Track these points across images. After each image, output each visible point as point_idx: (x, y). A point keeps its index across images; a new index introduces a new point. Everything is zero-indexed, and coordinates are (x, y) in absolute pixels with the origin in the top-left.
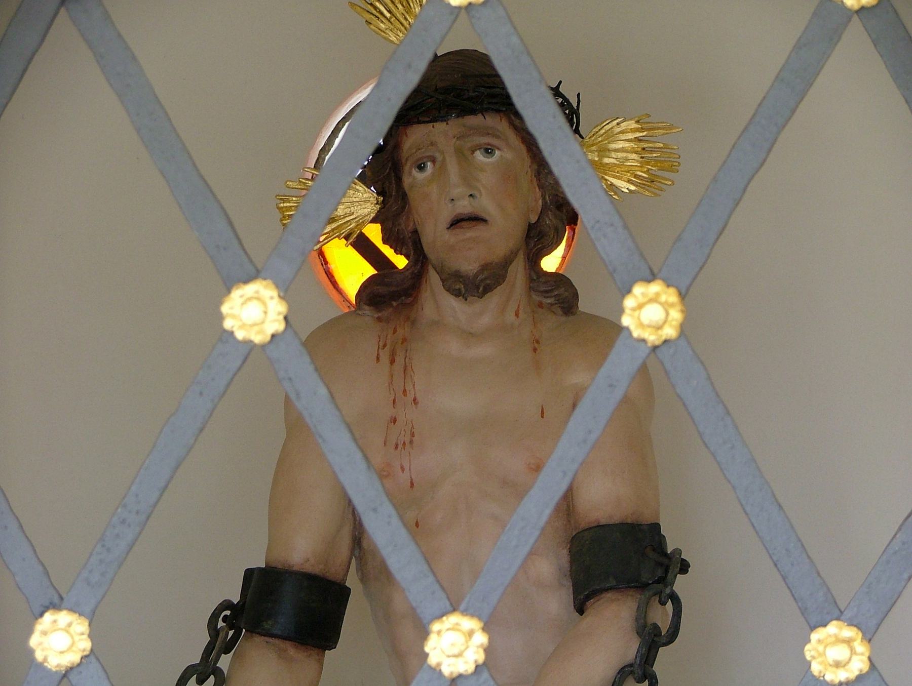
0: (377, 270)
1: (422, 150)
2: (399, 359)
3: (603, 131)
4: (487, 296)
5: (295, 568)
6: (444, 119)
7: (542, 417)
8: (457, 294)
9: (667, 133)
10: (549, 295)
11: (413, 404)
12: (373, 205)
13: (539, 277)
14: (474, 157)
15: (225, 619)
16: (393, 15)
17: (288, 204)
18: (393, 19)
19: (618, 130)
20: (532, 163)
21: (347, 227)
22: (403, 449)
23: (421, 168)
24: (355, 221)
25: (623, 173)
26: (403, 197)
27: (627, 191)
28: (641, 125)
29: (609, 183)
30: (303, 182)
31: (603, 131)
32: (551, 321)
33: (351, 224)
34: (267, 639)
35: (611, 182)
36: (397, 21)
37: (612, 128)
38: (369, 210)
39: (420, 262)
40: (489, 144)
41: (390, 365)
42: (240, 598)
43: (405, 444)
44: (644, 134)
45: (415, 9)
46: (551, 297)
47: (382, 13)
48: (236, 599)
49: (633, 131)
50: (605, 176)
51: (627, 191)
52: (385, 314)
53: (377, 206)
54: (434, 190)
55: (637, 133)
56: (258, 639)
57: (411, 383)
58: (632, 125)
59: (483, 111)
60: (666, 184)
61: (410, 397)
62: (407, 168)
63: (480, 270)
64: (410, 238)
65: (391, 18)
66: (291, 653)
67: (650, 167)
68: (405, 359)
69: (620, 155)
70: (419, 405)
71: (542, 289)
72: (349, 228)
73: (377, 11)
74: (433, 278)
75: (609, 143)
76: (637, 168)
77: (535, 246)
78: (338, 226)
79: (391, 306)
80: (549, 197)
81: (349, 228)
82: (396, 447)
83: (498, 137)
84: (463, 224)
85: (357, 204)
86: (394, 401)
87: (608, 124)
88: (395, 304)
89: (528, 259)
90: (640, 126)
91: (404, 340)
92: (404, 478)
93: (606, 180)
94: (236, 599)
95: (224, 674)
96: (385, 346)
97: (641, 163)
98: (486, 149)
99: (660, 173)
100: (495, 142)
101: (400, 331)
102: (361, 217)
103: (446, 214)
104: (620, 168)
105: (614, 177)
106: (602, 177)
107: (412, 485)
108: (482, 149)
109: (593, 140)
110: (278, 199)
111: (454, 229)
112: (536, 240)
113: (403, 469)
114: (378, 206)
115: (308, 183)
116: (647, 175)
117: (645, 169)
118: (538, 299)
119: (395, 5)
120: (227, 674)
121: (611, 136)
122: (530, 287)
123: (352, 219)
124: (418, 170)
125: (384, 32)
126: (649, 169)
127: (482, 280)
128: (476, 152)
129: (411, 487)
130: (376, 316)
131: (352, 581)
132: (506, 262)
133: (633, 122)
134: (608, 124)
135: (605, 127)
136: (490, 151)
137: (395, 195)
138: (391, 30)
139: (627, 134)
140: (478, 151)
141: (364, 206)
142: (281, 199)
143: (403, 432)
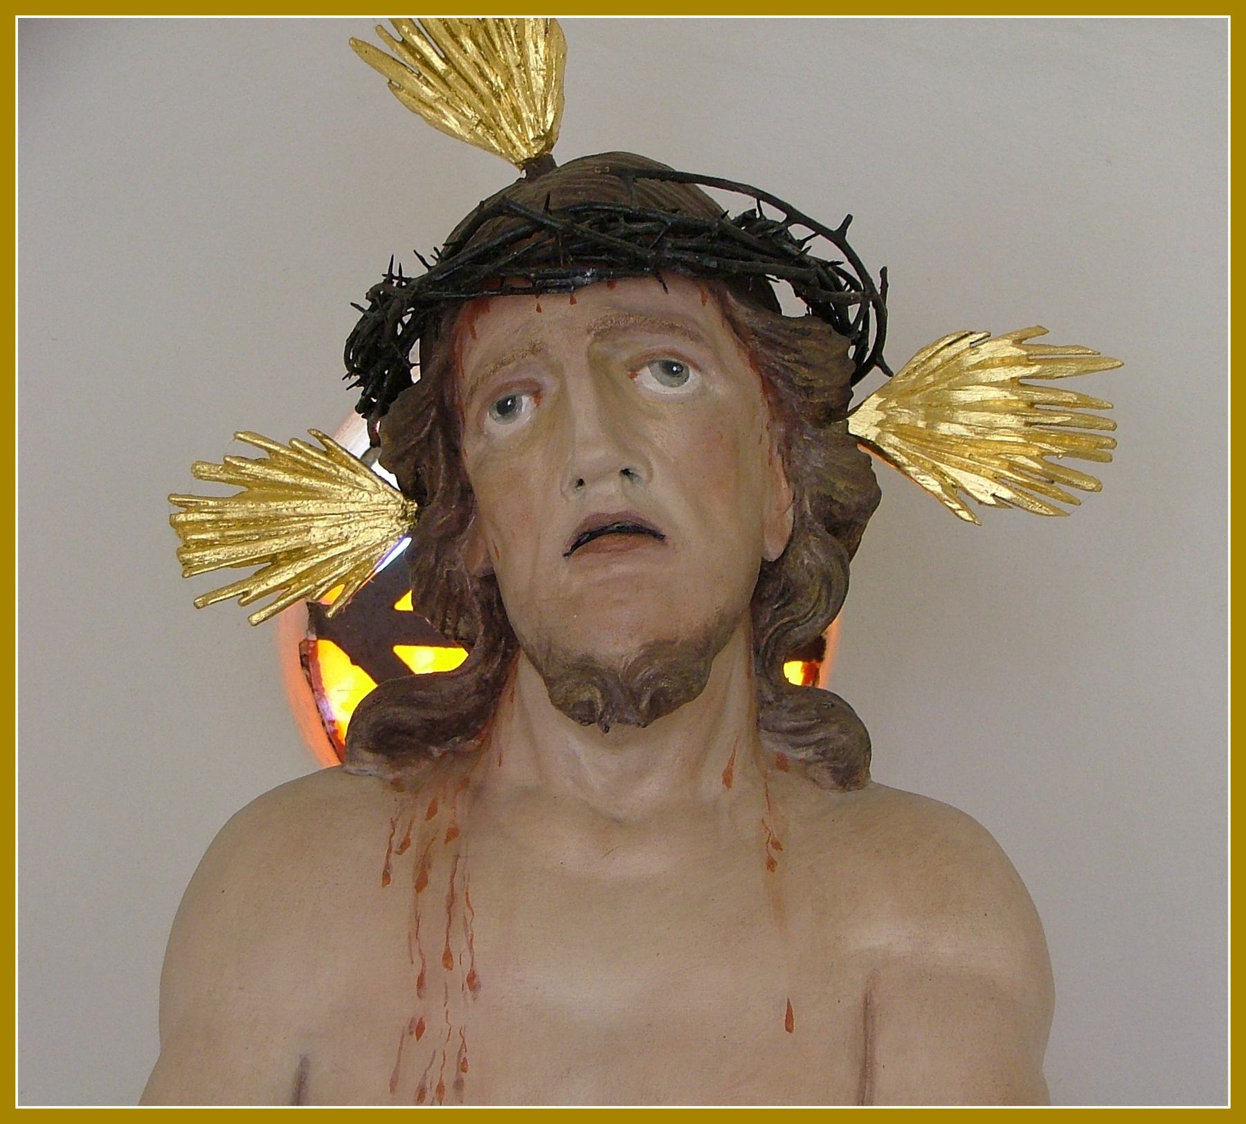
0: (397, 660)
1: (510, 366)
2: (438, 878)
3: (937, 361)
6: (567, 288)
7: (789, 1029)
8: (585, 715)
9: (1087, 372)
10: (802, 739)
11: (466, 986)
12: (393, 521)
13: (779, 697)
16: (455, 68)
17: (197, 517)
18: (452, 77)
19: (974, 359)
20: (773, 419)
23: (506, 409)
25: (982, 459)
27: (992, 501)
28: (1027, 351)
29: (949, 481)
31: (937, 361)
33: (341, 565)
35: (954, 480)
37: (958, 355)
38: (385, 532)
39: (501, 654)
40: (672, 353)
44: (1034, 369)
45: (504, 51)
46: (808, 745)
47: (427, 64)
49: (1005, 362)
50: (942, 466)
51: (992, 501)
52: (411, 773)
54: (536, 463)
55: (1018, 368)
58: (1008, 349)
59: (659, 271)
60: (1084, 489)
61: (461, 970)
62: (471, 414)
63: (643, 656)
64: (476, 593)
67: (1046, 446)
68: (452, 877)
69: (976, 417)
70: (481, 993)
71: (787, 725)
72: (337, 572)
73: (415, 58)
75: (951, 388)
76: (1016, 449)
78: (312, 568)
81: (337, 572)
83: (696, 338)
84: (604, 540)
85: (358, 518)
87: (950, 344)
88: (436, 751)
89: (757, 652)
91: (453, 833)
93: (943, 474)
96: (405, 845)
97: (1025, 436)
99: (1068, 462)
100: (686, 348)
101: (444, 812)
102: (365, 549)
104: (976, 447)
105: (962, 467)
106: (934, 467)
108: (656, 365)
109: (915, 381)
110: (175, 503)
115: (244, 468)
116: (1039, 464)
117: (1035, 452)
118: (776, 750)
119: (457, 42)
121: (957, 374)
123: (345, 553)
124: (499, 415)
126: (1043, 453)
127: (648, 682)
128: (641, 372)
130: (391, 776)
134: (950, 344)
136: (675, 369)
138: (447, 102)
139: (992, 370)
140: (647, 369)
141: (372, 523)
142: (180, 504)
143: (439, 1059)
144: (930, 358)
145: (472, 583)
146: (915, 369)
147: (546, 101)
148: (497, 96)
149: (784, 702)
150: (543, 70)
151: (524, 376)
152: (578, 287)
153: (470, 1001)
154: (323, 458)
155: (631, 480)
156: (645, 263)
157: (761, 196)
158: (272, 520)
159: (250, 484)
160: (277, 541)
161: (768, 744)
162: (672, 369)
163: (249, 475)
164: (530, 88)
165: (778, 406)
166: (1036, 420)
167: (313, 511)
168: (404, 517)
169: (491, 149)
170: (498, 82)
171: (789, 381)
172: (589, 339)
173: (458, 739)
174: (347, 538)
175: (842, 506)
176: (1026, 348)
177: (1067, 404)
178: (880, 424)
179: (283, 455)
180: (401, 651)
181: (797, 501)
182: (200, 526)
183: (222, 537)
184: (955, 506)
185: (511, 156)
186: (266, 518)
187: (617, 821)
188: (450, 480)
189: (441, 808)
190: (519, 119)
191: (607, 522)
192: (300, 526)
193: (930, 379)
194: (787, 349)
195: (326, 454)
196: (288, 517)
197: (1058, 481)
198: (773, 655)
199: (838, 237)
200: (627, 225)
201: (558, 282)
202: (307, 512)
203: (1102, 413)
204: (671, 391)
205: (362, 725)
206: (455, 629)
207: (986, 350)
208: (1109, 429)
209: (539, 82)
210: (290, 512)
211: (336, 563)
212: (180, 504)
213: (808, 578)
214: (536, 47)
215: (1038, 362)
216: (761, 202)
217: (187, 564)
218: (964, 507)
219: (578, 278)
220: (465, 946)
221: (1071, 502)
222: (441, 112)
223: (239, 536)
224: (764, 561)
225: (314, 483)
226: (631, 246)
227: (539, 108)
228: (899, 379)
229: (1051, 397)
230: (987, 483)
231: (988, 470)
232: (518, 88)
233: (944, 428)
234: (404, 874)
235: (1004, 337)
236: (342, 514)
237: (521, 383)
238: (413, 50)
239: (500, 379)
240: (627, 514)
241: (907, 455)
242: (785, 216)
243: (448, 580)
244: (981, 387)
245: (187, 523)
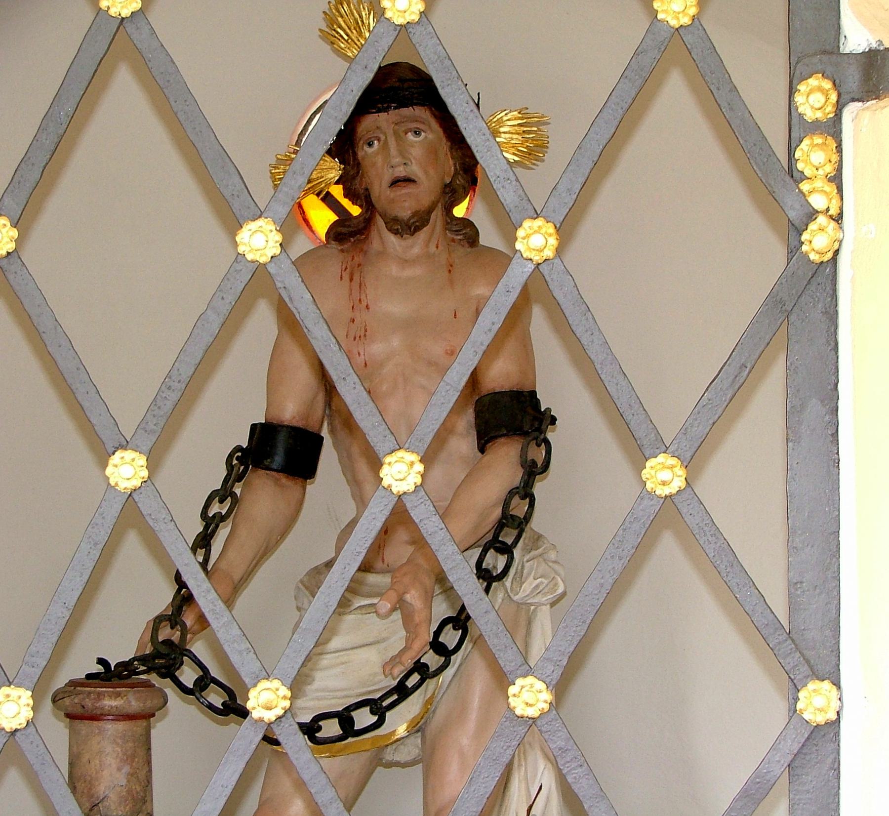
2: (356, 278)
6: (386, 110)
8: (396, 233)
17: (278, 171)
18: (350, 41)
23: (370, 145)
32: (461, 251)
46: (461, 235)
47: (341, 36)
48: (245, 445)
51: (513, 161)
54: (379, 160)
56: (261, 472)
61: (364, 304)
64: (363, 194)
65: (348, 40)
74: (380, 222)
86: (353, 307)
88: (352, 239)
91: (359, 265)
94: (245, 445)
96: (345, 269)
99: (535, 149)
103: (387, 178)
113: (359, 354)
121: (500, 122)
130: (340, 248)
131: (325, 433)
151: (375, 135)
161: (449, 234)
162: (417, 133)
187: (406, 261)
188: (354, 161)
203: (545, 133)
205: (332, 233)
207: (509, 116)
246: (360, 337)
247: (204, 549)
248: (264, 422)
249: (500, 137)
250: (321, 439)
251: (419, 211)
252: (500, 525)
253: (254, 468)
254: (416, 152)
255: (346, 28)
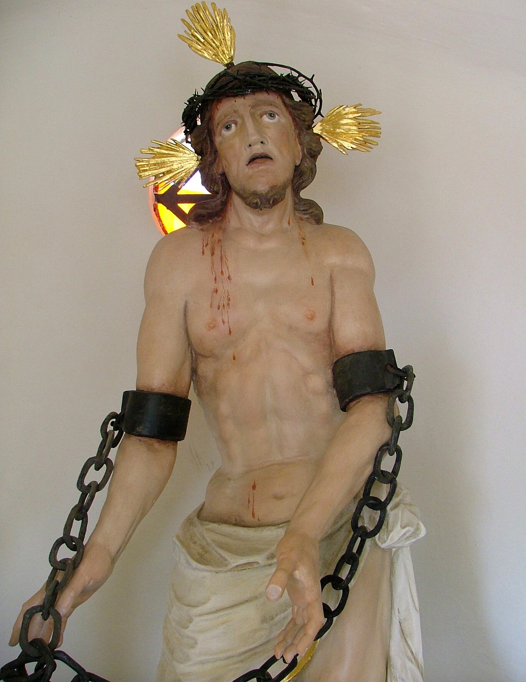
2: (217, 252)
4: (274, 207)
5: (156, 391)
6: (243, 95)
8: (255, 206)
10: (306, 212)
13: (299, 201)
14: (262, 119)
15: (112, 424)
16: (206, 40)
19: (344, 112)
20: (295, 129)
21: (179, 176)
22: (223, 310)
23: (228, 128)
24: (184, 171)
25: (348, 138)
26: (215, 152)
27: (351, 149)
28: (357, 110)
29: (340, 144)
30: (151, 149)
32: (309, 228)
34: (140, 438)
35: (341, 143)
36: (208, 44)
37: (340, 112)
38: (193, 165)
39: (226, 195)
41: (211, 256)
42: (122, 410)
43: (229, 305)
45: (219, 35)
46: (308, 214)
47: (198, 40)
48: (119, 412)
51: (351, 149)
52: (205, 227)
53: (197, 162)
54: (237, 142)
55: (355, 114)
56: (134, 439)
57: (226, 267)
59: (267, 90)
62: (217, 132)
65: (204, 42)
66: (156, 446)
68: (221, 252)
71: (302, 209)
74: (236, 200)
77: (298, 181)
79: (209, 222)
80: (306, 150)
82: (219, 309)
83: (277, 107)
84: (257, 160)
86: (215, 279)
88: (211, 221)
90: (357, 110)
91: (219, 241)
92: (224, 328)
93: (338, 142)
94: (119, 412)
95: (113, 464)
96: (207, 245)
97: (358, 132)
98: (271, 113)
102: (188, 169)
103: (246, 155)
106: (336, 140)
107: (230, 332)
109: (329, 118)
111: (252, 164)
112: (298, 178)
113: (224, 322)
114: (198, 162)
120: (115, 462)
121: (341, 116)
122: (295, 208)
123: (182, 171)
125: (201, 51)
126: (363, 136)
127: (272, 196)
128: (263, 116)
129: (229, 334)
130: (200, 228)
131: (192, 396)
132: (284, 188)
133: (353, 108)
134: (337, 109)
135: (336, 111)
137: (210, 151)
141: (190, 162)
142: (138, 160)
143: (222, 299)
144: (333, 113)
145: (218, 176)
146: (329, 116)
147: (231, 48)
148: (218, 48)
149: (301, 203)
150: (230, 40)
152: (247, 94)
153: (229, 283)
154: (175, 146)
155: (263, 144)
156: (264, 87)
157: (292, 69)
158: (162, 163)
159: (156, 154)
160: (164, 168)
161: (297, 214)
162: (272, 115)
163: (156, 152)
164: (227, 45)
165: (296, 125)
166: (361, 127)
167: (173, 160)
168: (198, 160)
169: (217, 61)
170: (218, 44)
171: (299, 118)
172: (250, 108)
173: (216, 217)
174: (183, 167)
175: (314, 151)
176: (357, 109)
177: (369, 123)
178: (321, 130)
179: (164, 146)
180: (179, 205)
181: (303, 150)
182: (143, 166)
183: (150, 168)
184: (342, 150)
185: (223, 63)
186: (161, 163)
188: (211, 148)
189: (215, 235)
190: (224, 53)
191: (258, 155)
192: (170, 164)
193: (333, 118)
194: (299, 110)
195: (176, 145)
196: (167, 162)
197: (367, 143)
198: (298, 191)
199: (311, 80)
200: (259, 78)
201: (241, 93)
202: (172, 160)
204: (271, 121)
206: (214, 189)
207: (347, 110)
208: (379, 129)
209: (229, 43)
210: (167, 161)
211: (180, 174)
212: (138, 160)
213: (307, 170)
214: (228, 34)
215: (360, 113)
216: (292, 71)
217: (140, 176)
218: (344, 150)
219: (247, 92)
220: (226, 269)
221: (370, 148)
222: (203, 52)
223: (154, 168)
224: (296, 166)
225: (171, 152)
226: (261, 83)
227: (229, 50)
228: (325, 118)
229: (365, 122)
230: (349, 144)
231: (350, 141)
232: (223, 45)
233: (338, 130)
234: (208, 252)
235: (351, 107)
236: (181, 160)
237: (232, 121)
238: (195, 36)
239: (226, 120)
240: (263, 153)
241: (329, 138)
242: (298, 75)
243: (212, 175)
244: (347, 119)
245: (140, 165)
246: (224, 306)
247: (81, 521)
248: (135, 390)
249: (339, 128)
250: (189, 402)
251: (276, 186)
252: (370, 483)
253: (126, 434)
254: (271, 133)
255: (202, 32)
